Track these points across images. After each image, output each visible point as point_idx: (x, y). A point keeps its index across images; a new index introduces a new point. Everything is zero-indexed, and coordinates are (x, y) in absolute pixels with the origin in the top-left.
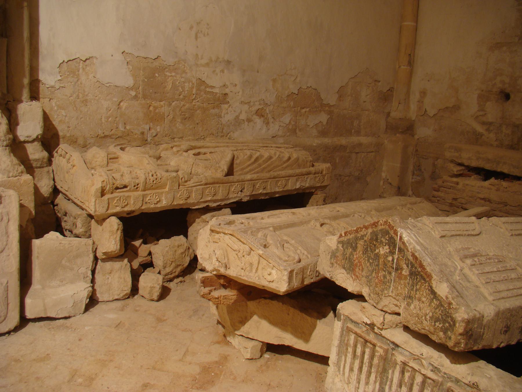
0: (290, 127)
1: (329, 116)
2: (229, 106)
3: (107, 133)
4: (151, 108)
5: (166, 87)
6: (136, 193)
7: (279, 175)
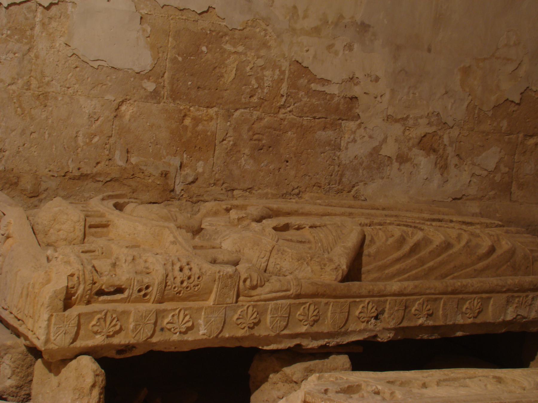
2: (359, 126)
3: (86, 170)
4: (187, 121)
5: (222, 76)
6: (142, 307)
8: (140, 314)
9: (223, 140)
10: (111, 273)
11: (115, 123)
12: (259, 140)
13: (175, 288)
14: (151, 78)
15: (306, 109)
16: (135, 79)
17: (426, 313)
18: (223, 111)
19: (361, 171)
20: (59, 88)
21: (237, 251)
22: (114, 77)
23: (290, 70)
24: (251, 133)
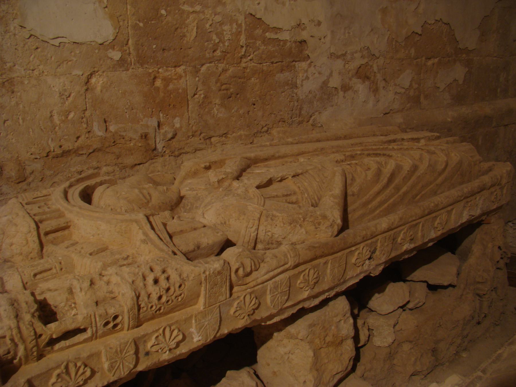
0: (412, 93)
1: (467, 70)
2: (310, 65)
3: (68, 146)
4: (158, 83)
5: (185, 36)
6: (114, 341)
7: (437, 205)
8: (114, 350)
9: (195, 95)
10: (69, 303)
11: (87, 96)
12: (227, 90)
13: (152, 307)
14: (115, 47)
15: (264, 56)
16: (99, 50)
17: (409, 238)
18: (190, 68)
19: (315, 103)
20: (23, 72)
21: (222, 223)
22: (78, 52)
23: (245, 22)
24: (219, 84)
